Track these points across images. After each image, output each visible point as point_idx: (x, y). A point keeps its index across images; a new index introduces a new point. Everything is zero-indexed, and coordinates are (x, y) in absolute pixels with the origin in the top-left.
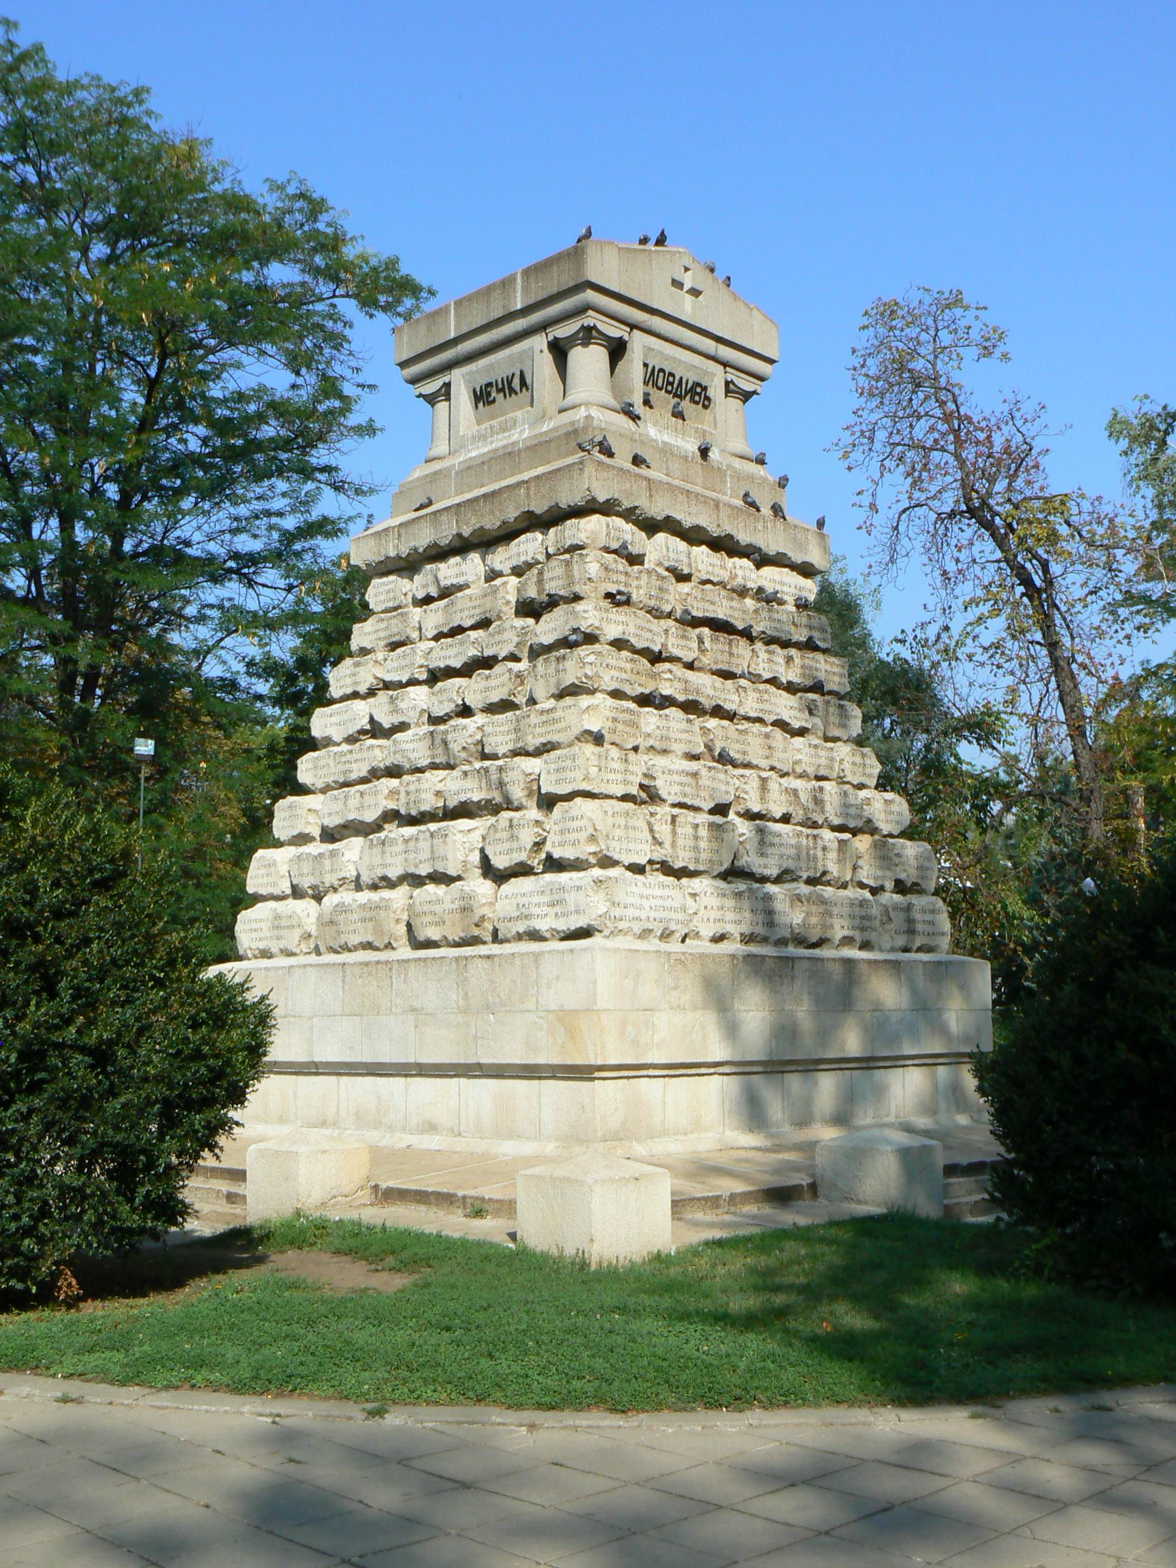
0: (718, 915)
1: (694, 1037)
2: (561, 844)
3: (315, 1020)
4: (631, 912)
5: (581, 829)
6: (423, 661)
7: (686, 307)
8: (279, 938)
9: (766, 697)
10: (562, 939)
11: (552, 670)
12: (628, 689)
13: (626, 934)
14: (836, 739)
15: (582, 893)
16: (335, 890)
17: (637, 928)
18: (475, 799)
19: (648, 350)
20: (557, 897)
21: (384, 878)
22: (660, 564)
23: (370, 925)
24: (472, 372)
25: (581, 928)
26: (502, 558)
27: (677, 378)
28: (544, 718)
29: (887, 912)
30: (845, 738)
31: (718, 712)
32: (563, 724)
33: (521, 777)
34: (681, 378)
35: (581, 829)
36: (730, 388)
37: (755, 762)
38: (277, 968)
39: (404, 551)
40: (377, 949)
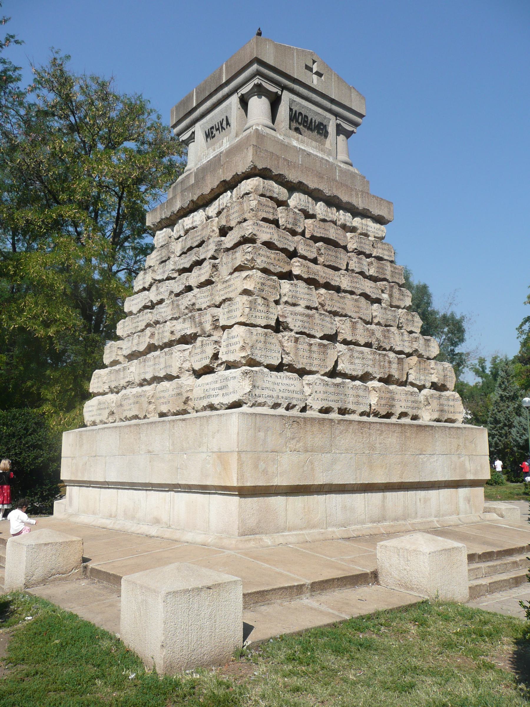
0: (324, 396)
1: (305, 468)
2: (227, 353)
3: (107, 458)
4: (266, 392)
5: (236, 343)
6: (173, 267)
7: (315, 81)
8: (100, 415)
9: (356, 280)
10: (227, 409)
11: (230, 260)
12: (272, 268)
13: (264, 406)
14: (398, 307)
15: (236, 380)
16: (125, 388)
17: (270, 402)
18: (188, 333)
19: (292, 102)
20: (223, 384)
21: (145, 380)
22: (296, 207)
23: (137, 406)
24: (204, 123)
25: (235, 401)
26: (212, 210)
27: (309, 119)
28: (224, 285)
29: (427, 399)
30: (403, 306)
31: (328, 286)
32: (233, 287)
33: (210, 318)
34: (312, 119)
35: (236, 343)
36: (340, 130)
37: (349, 314)
38: (89, 430)
39: (168, 214)
40: (140, 419)
